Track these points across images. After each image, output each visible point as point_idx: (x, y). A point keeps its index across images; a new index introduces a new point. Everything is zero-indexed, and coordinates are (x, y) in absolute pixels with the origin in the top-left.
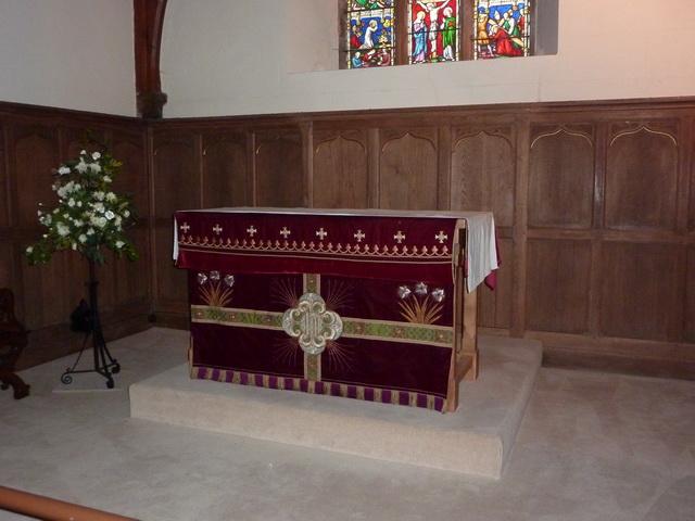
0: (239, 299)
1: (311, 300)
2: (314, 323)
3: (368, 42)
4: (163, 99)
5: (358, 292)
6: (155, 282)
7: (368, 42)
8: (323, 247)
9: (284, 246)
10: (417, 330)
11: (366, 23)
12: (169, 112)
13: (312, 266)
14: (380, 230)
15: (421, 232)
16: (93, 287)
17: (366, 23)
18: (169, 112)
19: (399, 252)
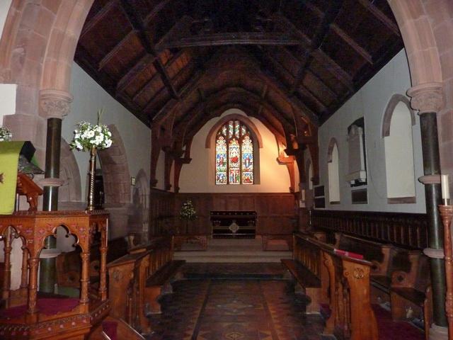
0: (222, 225)
1: (234, 224)
2: (234, 227)
3: (221, 178)
4: (179, 189)
5: (240, 222)
6: (130, 312)
7: (221, 178)
8: (236, 216)
9: (230, 216)
10: (250, 227)
11: (220, 175)
12: (180, 191)
13: (233, 219)
14: (245, 213)
15: (251, 213)
16: (124, 70)
17: (220, 175)
18: (180, 191)
19: (248, 216)
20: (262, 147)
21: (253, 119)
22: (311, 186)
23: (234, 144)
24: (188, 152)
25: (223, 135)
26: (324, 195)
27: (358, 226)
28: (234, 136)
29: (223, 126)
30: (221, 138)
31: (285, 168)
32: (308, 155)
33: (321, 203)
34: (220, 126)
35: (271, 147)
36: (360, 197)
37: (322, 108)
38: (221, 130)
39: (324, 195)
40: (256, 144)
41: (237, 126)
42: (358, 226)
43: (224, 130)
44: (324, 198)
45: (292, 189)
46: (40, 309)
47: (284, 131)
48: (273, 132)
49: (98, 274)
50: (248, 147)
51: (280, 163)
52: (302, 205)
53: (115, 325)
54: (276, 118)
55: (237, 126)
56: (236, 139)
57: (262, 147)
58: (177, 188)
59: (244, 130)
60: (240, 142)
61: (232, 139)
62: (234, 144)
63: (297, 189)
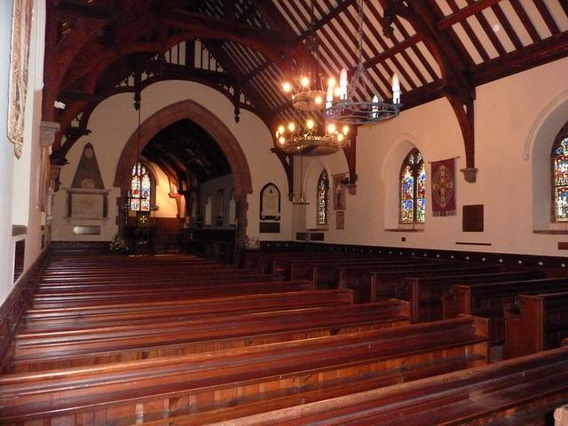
21: (153, 164)
22: (194, 214)
24: (84, 122)
26: (261, 223)
27: (229, 47)
28: (136, 174)
31: (174, 200)
32: (194, 195)
33: (201, 225)
35: (165, 185)
36: (220, 224)
39: (261, 223)
40: (154, 182)
41: (139, 167)
42: (229, 47)
44: (279, 224)
45: (178, 215)
47: (179, 177)
48: (167, 175)
49: (443, 167)
50: (146, 184)
51: (171, 197)
52: (185, 227)
55: (139, 167)
59: (144, 170)
63: (182, 216)
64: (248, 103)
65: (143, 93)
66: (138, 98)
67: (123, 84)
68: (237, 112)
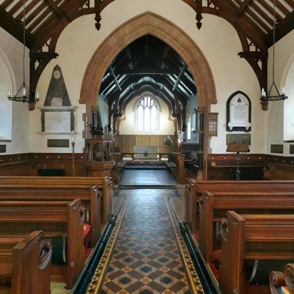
20: (83, 148)
23: (147, 109)
24: (52, 47)
25: (142, 105)
28: (147, 106)
29: (142, 100)
30: (140, 106)
34: (140, 100)
37: (117, 156)
38: (140, 102)
43: (142, 101)
46: (101, 158)
53: (144, 246)
54: (216, 192)
56: (148, 107)
57: (83, 148)
58: (118, 132)
60: (150, 108)
61: (146, 107)
62: (147, 109)
64: (212, 6)
65: (102, 14)
66: (98, 19)
67: (85, 6)
68: (199, 18)
